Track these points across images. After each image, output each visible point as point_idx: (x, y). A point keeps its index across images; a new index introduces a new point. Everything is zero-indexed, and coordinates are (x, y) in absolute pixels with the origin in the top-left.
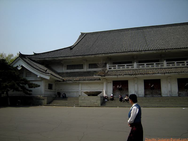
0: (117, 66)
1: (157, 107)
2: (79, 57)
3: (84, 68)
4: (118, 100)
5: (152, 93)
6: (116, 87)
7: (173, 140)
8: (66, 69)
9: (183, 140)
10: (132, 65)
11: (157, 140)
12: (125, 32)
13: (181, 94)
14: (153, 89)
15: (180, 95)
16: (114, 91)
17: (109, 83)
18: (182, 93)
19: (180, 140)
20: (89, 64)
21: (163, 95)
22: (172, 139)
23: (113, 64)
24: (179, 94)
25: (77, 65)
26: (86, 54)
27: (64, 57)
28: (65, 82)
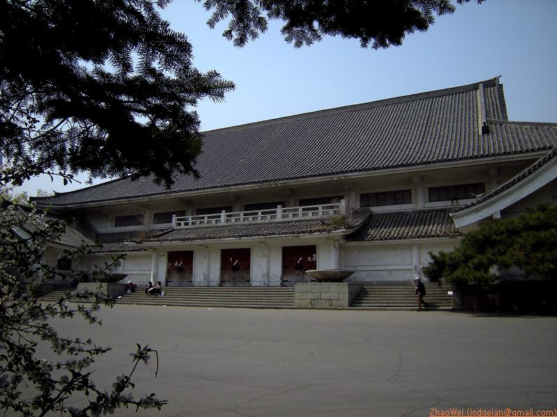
0: (260, 213)
1: (188, 306)
2: (306, 179)
3: (413, 201)
4: (415, 301)
5: (234, 278)
6: (173, 264)
7: (511, 415)
8: (114, 225)
9: (543, 413)
10: (272, 212)
11: (465, 415)
12: (457, 96)
13: (287, 281)
14: (235, 269)
15: (286, 283)
16: (169, 272)
17: (161, 256)
18: (289, 279)
19: (535, 414)
20: (430, 189)
21: (254, 284)
22: (509, 410)
23: (197, 214)
24: (284, 281)
25: (377, 194)
26: (338, 170)
27: (97, 201)
28: (92, 255)
